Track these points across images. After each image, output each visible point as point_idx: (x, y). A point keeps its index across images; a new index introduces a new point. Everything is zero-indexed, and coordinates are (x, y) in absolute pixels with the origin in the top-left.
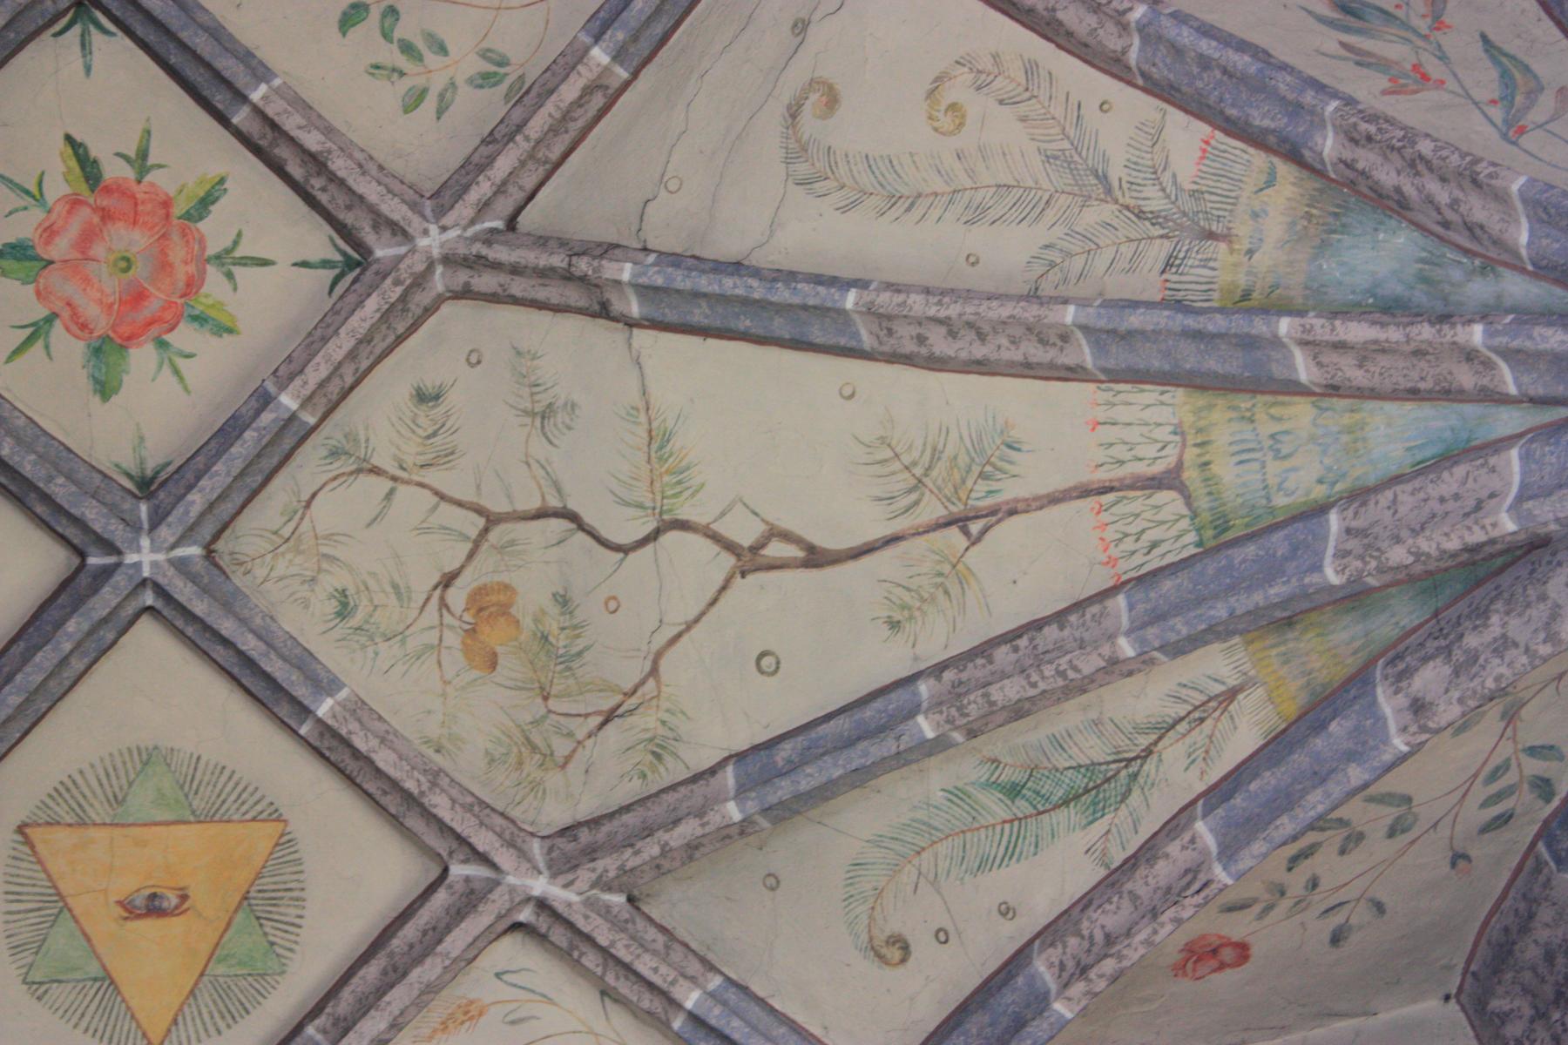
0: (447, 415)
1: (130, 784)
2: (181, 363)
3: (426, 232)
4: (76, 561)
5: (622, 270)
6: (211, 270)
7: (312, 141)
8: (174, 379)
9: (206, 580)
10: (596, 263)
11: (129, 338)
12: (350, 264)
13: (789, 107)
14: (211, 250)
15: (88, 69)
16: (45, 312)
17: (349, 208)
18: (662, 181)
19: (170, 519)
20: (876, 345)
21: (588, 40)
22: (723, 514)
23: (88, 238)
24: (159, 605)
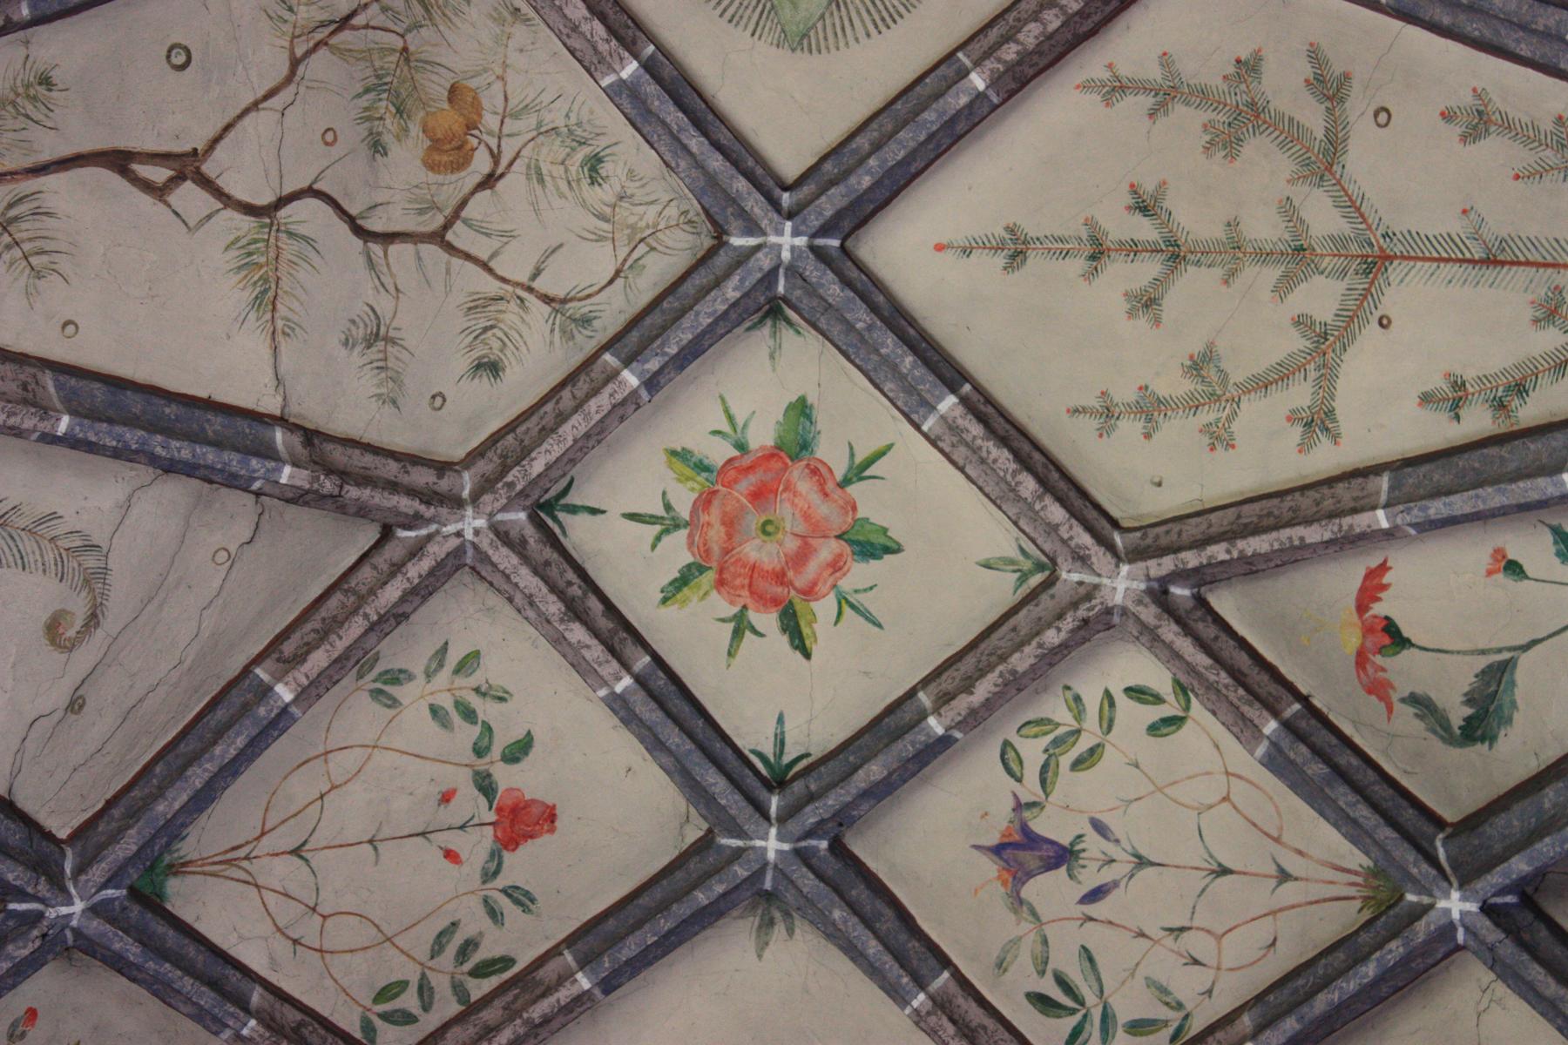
0: (471, 348)
1: (822, 17)
2: (726, 428)
3: (477, 532)
4: (849, 243)
5: (291, 477)
6: (685, 514)
7: (577, 633)
8: (734, 411)
9: (730, 210)
10: (316, 486)
11: (772, 456)
12: (549, 507)
13: (97, 625)
14: (683, 534)
15: (780, 720)
16: (849, 489)
17: (547, 563)
18: (233, 561)
19: (759, 275)
20: (39, 375)
21: (293, 709)
22: (209, 217)
23: (801, 557)
24: (777, 191)
